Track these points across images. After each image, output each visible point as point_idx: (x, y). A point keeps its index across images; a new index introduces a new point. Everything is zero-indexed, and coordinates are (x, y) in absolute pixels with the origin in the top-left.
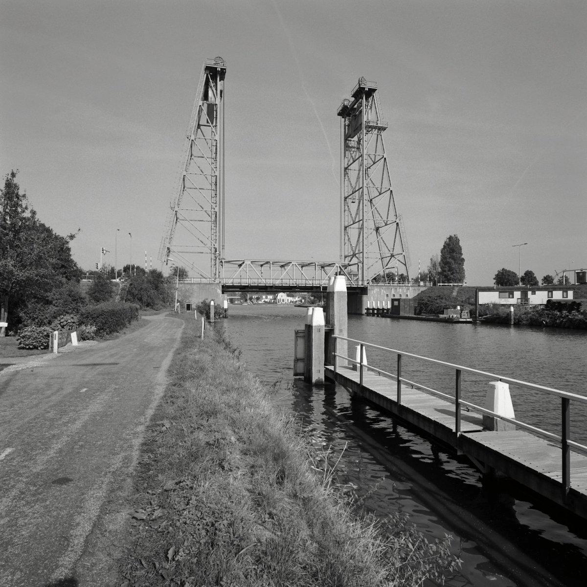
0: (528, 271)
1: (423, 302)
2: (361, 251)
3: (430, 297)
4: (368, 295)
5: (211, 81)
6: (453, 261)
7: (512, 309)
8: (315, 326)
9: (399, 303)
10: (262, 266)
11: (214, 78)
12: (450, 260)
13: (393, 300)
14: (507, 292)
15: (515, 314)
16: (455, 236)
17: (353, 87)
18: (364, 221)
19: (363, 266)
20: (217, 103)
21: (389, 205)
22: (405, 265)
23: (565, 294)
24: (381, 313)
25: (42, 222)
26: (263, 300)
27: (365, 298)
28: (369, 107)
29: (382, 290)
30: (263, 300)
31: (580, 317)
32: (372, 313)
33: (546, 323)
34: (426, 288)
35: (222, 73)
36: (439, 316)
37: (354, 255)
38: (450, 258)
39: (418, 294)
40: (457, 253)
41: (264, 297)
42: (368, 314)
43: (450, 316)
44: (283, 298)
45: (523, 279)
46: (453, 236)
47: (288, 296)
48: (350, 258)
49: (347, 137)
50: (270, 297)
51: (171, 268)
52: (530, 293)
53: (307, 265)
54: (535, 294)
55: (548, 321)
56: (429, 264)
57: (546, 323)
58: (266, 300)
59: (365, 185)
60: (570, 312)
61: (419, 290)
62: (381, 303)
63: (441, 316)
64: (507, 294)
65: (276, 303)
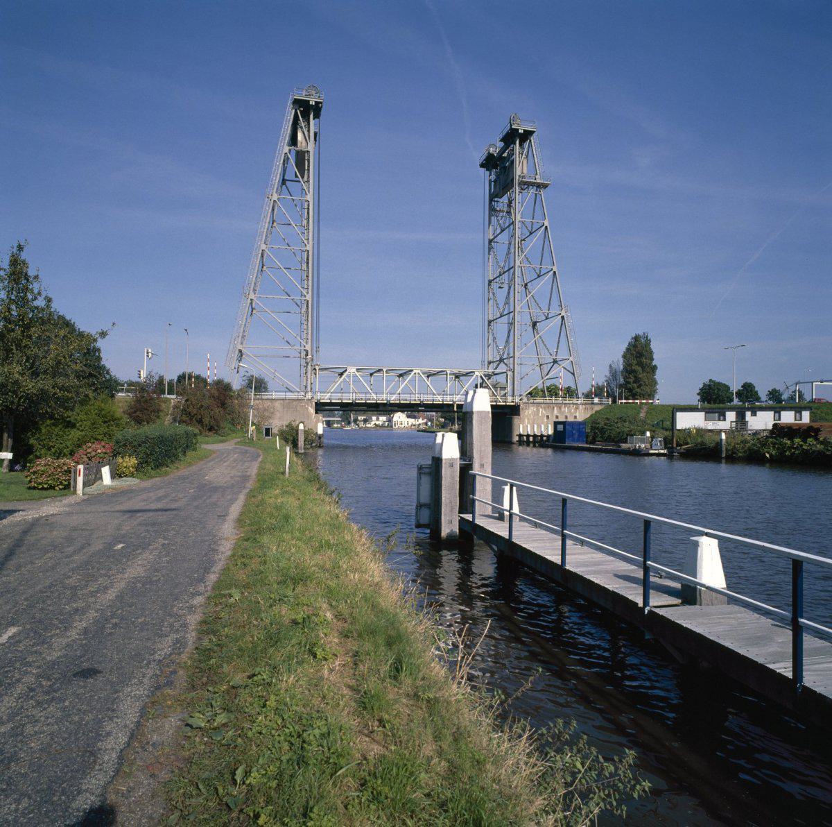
2: (512, 355)
3: (608, 419)
6: (640, 369)
7: (723, 436)
8: (446, 459)
10: (371, 375)
11: (306, 116)
13: (556, 424)
14: (715, 413)
16: (644, 334)
22: (573, 374)
24: (539, 441)
25: (61, 314)
26: (373, 423)
27: (516, 420)
28: (524, 156)
30: (373, 423)
31: (820, 447)
32: (525, 441)
33: (771, 455)
34: (603, 406)
35: (317, 110)
36: (620, 447)
37: (501, 360)
41: (374, 418)
42: (521, 442)
43: (635, 446)
46: (641, 334)
47: (408, 417)
48: (495, 365)
49: (493, 197)
50: (383, 419)
51: (244, 378)
52: (748, 414)
53: (435, 374)
54: (756, 415)
55: (774, 453)
56: (608, 374)
57: (771, 455)
58: (377, 423)
59: (518, 263)
60: (804, 440)
62: (533, 428)
63: (624, 446)
64: (717, 414)
65: (392, 427)
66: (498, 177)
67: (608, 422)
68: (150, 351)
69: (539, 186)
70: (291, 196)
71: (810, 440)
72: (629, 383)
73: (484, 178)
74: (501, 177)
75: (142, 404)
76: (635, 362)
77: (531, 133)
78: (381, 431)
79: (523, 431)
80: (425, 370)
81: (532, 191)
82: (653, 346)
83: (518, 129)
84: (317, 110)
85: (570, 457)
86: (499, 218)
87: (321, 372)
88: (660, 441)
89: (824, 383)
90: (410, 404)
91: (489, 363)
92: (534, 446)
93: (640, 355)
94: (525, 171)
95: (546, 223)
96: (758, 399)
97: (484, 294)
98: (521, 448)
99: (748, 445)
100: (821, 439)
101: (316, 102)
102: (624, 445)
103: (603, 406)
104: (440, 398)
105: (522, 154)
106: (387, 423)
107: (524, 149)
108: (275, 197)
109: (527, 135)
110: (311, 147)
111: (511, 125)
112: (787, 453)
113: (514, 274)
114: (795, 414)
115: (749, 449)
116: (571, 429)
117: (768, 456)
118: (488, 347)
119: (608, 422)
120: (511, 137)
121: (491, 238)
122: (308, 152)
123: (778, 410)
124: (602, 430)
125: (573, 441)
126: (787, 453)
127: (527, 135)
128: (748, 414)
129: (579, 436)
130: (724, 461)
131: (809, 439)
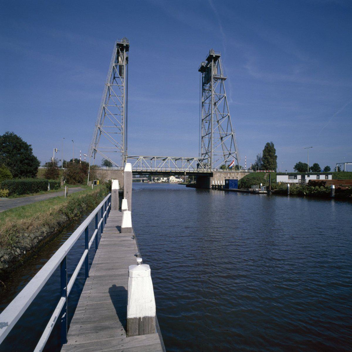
0: (315, 163)
1: (243, 181)
2: (210, 151)
3: (248, 178)
4: (214, 177)
5: (120, 51)
6: (270, 157)
7: (289, 185)
8: (113, 190)
9: (229, 182)
10: (151, 159)
11: (122, 50)
12: (268, 157)
13: (226, 180)
14: (293, 176)
15: (291, 188)
16: (271, 142)
17: (207, 55)
18: (212, 133)
19: (211, 160)
20: (123, 65)
21: (228, 124)
22: (237, 159)
23: (326, 176)
24: (219, 188)
25: (15, 134)
26: (161, 181)
27: (211, 179)
28: (216, 67)
29: (222, 174)
30: (161, 181)
31: (324, 190)
32: (215, 188)
33: (306, 193)
34: (249, 173)
35: (127, 48)
36: (248, 190)
37: (207, 153)
38: (268, 155)
39: (244, 177)
40: (272, 153)
41: (162, 178)
42: (213, 188)
43: (254, 190)
44: (173, 179)
45: (312, 168)
46: (270, 142)
47: (176, 178)
48: (204, 155)
49: (204, 84)
50: (165, 179)
51: (103, 161)
52: (306, 176)
53: (178, 159)
54: (309, 177)
55: (307, 192)
56: (256, 159)
57: (306, 193)
58: (163, 180)
59: (213, 112)
60: (319, 187)
61: (245, 174)
62: (220, 182)
63: (250, 189)
64: (293, 176)
65: (169, 182)
66: (205, 75)
67: (248, 180)
68: (56, 149)
69: (222, 79)
70: (118, 84)
71: (322, 187)
72: (265, 163)
73: (200, 76)
74: (207, 76)
75: (51, 172)
76: (267, 154)
77: (219, 57)
78: (165, 183)
79: (214, 184)
80: (173, 157)
81: (219, 81)
82: (275, 147)
83: (213, 55)
84: (127, 48)
85: (232, 196)
86: (206, 93)
87: (129, 158)
88: (265, 188)
89: (348, 164)
90: (180, 172)
91: (202, 154)
92: (218, 190)
93: (270, 151)
94: (216, 73)
95: (225, 95)
96: (320, 171)
97: (200, 125)
98: (213, 191)
99: (298, 189)
100: (326, 186)
101: (126, 45)
102: (250, 189)
103: (249, 173)
104: (179, 169)
105: (215, 66)
106: (167, 181)
107: (216, 64)
108: (109, 85)
109: (217, 58)
110: (124, 63)
111: (210, 54)
112: (312, 192)
113: (211, 117)
114: (326, 177)
115: (299, 191)
116: (231, 183)
117: (305, 193)
118: (202, 148)
119: (248, 180)
120: (210, 58)
121: (203, 101)
122: (123, 66)
123: (318, 174)
124: (245, 183)
125: (232, 188)
126: (312, 192)
127: (217, 58)
128: (306, 176)
129: (235, 186)
130: (289, 196)
131: (321, 187)
